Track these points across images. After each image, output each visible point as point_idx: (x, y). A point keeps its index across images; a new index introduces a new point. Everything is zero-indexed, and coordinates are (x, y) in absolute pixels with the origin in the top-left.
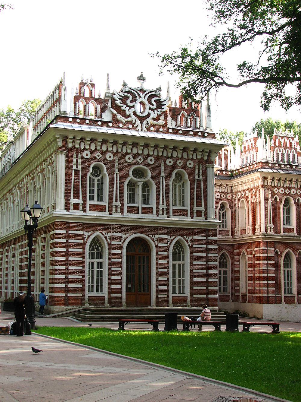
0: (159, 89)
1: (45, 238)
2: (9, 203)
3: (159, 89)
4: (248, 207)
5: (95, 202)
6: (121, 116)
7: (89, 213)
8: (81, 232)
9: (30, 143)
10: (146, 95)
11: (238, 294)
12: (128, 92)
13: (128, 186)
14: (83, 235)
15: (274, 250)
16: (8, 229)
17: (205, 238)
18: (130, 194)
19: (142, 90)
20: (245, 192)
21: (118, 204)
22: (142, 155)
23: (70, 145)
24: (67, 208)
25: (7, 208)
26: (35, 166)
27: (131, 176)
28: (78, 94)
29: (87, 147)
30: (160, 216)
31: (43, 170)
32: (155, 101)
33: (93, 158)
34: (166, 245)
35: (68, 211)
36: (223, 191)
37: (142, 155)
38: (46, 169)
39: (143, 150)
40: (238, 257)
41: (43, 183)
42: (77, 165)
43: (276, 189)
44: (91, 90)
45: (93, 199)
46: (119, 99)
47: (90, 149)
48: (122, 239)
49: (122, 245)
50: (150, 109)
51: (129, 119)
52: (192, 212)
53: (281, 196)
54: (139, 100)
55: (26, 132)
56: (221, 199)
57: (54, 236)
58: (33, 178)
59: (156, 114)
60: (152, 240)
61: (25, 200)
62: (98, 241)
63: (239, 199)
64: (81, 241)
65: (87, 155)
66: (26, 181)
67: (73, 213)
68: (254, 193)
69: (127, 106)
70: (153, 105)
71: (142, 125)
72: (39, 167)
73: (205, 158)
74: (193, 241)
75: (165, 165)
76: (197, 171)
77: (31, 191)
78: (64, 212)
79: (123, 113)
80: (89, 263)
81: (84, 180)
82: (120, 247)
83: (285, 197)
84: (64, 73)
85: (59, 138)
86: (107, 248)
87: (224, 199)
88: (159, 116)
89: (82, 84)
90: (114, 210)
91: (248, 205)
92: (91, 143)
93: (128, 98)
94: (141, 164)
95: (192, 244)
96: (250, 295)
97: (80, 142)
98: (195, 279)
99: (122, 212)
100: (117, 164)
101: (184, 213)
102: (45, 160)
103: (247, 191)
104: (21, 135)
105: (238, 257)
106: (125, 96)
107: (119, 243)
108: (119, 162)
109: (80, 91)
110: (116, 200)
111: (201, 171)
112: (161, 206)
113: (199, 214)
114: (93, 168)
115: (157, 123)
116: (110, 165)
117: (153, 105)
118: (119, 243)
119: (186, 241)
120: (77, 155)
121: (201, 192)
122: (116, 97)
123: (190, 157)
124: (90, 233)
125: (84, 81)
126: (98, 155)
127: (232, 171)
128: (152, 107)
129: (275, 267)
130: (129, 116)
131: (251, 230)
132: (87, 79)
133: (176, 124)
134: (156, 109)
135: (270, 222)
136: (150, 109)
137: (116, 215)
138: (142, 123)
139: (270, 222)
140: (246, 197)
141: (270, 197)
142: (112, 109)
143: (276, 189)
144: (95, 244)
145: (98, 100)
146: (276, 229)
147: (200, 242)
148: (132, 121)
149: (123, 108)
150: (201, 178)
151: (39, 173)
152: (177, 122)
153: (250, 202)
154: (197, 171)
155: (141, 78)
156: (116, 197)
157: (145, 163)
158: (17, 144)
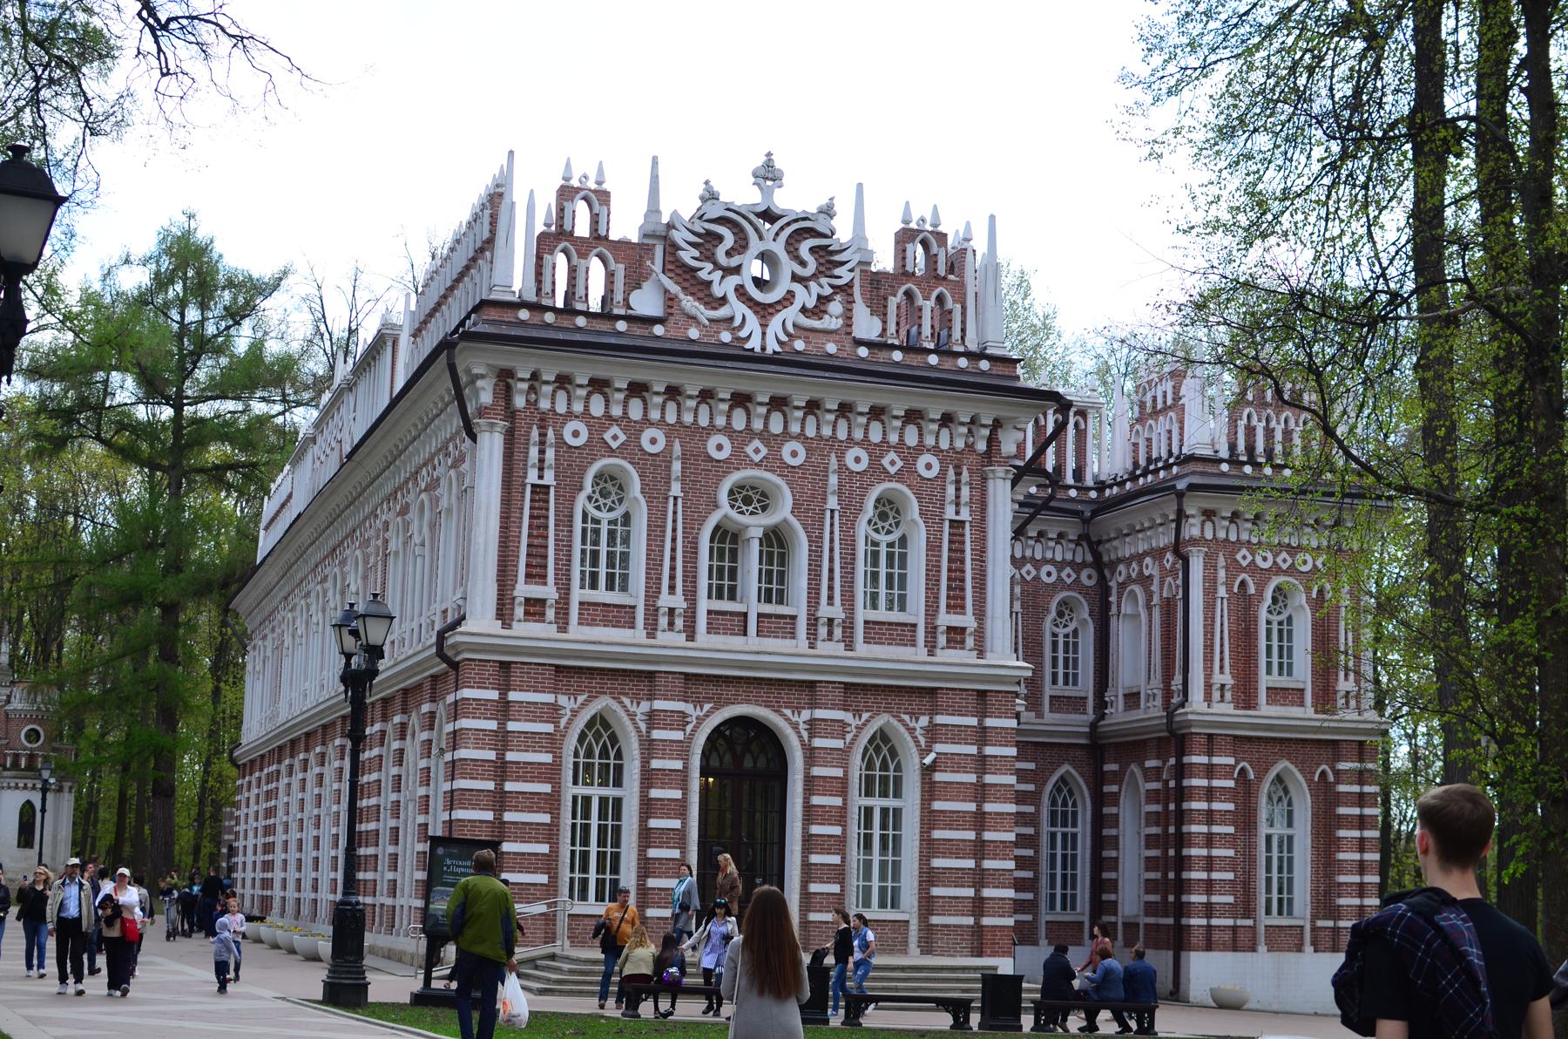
0: (828, 211)
1: (432, 715)
2: (330, 594)
3: (828, 211)
4: (1150, 615)
5: (602, 595)
6: (697, 304)
7: (576, 631)
8: (548, 698)
9: (400, 384)
10: (782, 229)
11: (1113, 919)
12: (721, 220)
13: (712, 540)
14: (683, 714)
15: (1233, 767)
16: (325, 682)
17: (973, 721)
18: (721, 570)
19: (769, 216)
20: (1140, 563)
21: (678, 602)
22: (765, 436)
23: (519, 402)
24: (504, 613)
25: (324, 611)
26: (410, 468)
27: (725, 508)
28: (553, 228)
29: (578, 407)
30: (819, 644)
31: (433, 485)
32: (812, 250)
33: (597, 446)
34: (839, 744)
35: (507, 625)
36: (1069, 556)
37: (765, 436)
38: (442, 482)
39: (767, 418)
40: (1114, 788)
41: (433, 526)
42: (541, 469)
43: (1244, 551)
44: (598, 215)
45: (594, 586)
46: (690, 244)
47: (586, 415)
48: (688, 723)
49: (690, 739)
50: (795, 278)
51: (722, 312)
52: (932, 631)
53: (1263, 576)
54: (755, 245)
55: (390, 344)
56: (1276, 570)
57: (456, 711)
58: (404, 511)
59: (815, 297)
60: (788, 724)
61: (379, 580)
62: (606, 725)
63: (1122, 586)
64: (549, 728)
65: (576, 433)
66: (384, 517)
67: (526, 631)
68: (1168, 566)
69: (717, 266)
70: (803, 264)
71: (764, 334)
72: (424, 472)
73: (981, 446)
74: (653, 718)
75: (842, 468)
76: (951, 490)
77: (397, 553)
78: (496, 627)
79: (702, 290)
80: (575, 798)
81: (566, 520)
82: (682, 749)
83: (1276, 581)
84: (511, 153)
85: (482, 377)
86: (636, 753)
87: (1069, 588)
88: (823, 300)
89: (566, 194)
90: (663, 621)
91: (1149, 608)
92: (589, 394)
93: (720, 238)
94: (758, 465)
95: (650, 728)
96: (1151, 920)
97: (554, 391)
98: (938, 863)
99: (691, 633)
100: (677, 467)
101: (902, 633)
102: (440, 450)
103: (1148, 560)
104: (374, 359)
105: (1114, 788)
106: (709, 233)
107: (678, 735)
108: (684, 459)
109: (561, 217)
110: (672, 588)
111: (965, 492)
112: (825, 611)
113: (956, 636)
114: (599, 477)
115: (816, 324)
116: (654, 470)
117: (803, 264)
118: (678, 735)
119: (907, 730)
120: (543, 435)
121: (963, 561)
122: (679, 236)
123: (930, 441)
124: (581, 699)
125: (575, 183)
126: (615, 436)
127: (1101, 486)
128: (799, 270)
129: (1234, 823)
130: (723, 300)
131: (1159, 693)
132: (584, 171)
133: (884, 330)
134: (814, 277)
135: (1222, 667)
136: (795, 278)
137: (671, 640)
138: (764, 326)
139: (1222, 667)
140: (1145, 581)
141: (1222, 574)
142: (662, 277)
143: (1244, 551)
144: (878, 750)
145: (622, 248)
146: (1245, 694)
147: (957, 734)
148: (732, 319)
149: (703, 275)
150: (965, 515)
151: (421, 492)
152: (884, 322)
153: (1156, 600)
154: (951, 490)
155: (768, 174)
156: (672, 577)
157: (773, 462)
158: (362, 387)
